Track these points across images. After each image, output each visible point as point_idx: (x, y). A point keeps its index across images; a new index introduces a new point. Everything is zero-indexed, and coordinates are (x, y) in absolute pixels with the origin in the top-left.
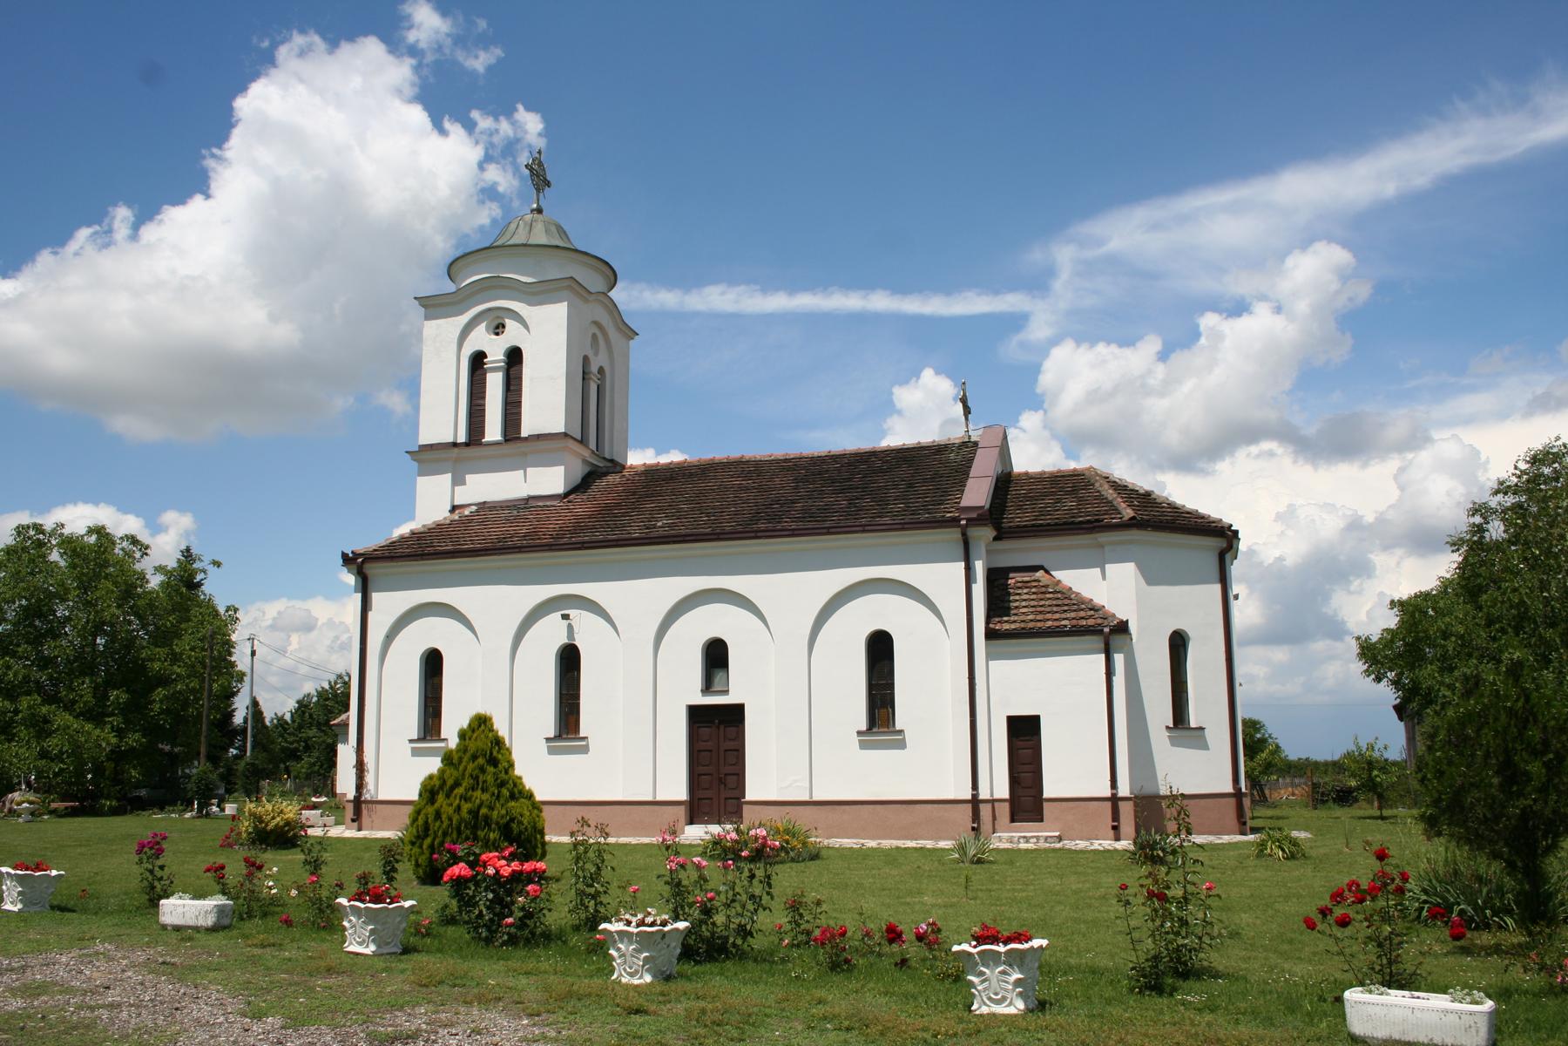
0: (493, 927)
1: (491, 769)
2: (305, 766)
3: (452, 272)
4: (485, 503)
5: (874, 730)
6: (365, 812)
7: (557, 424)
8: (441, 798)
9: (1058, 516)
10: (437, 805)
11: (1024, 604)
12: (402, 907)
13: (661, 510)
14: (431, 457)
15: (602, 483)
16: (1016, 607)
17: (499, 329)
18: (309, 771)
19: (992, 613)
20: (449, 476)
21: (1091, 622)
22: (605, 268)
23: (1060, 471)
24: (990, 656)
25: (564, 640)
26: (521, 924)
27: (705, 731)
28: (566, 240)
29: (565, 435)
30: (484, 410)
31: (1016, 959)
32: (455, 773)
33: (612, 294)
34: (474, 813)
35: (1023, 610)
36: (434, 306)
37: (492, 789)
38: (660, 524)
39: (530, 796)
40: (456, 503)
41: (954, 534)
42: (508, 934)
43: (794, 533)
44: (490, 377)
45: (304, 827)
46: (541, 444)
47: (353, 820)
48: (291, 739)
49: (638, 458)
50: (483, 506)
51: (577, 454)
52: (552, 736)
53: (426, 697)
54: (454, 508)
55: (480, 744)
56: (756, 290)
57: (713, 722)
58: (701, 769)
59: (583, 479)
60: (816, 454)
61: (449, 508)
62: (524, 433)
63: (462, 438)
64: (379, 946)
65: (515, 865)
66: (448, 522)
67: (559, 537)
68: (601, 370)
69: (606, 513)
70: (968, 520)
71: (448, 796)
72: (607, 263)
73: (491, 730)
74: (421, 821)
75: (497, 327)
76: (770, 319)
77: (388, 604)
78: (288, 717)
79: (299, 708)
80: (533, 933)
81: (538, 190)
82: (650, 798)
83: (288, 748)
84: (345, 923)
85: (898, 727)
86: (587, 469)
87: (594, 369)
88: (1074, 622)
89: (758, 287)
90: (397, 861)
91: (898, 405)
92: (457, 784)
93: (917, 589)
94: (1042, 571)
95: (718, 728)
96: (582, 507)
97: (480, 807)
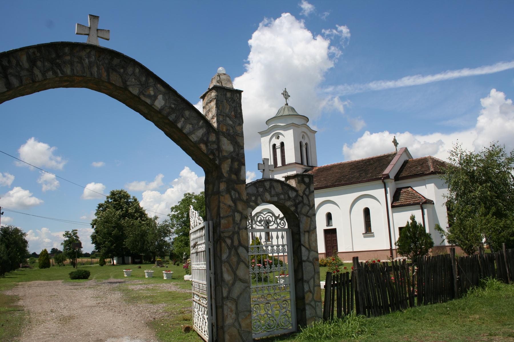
3: (267, 123)
5: (368, 233)
7: (293, 161)
9: (414, 172)
11: (403, 197)
16: (401, 199)
21: (418, 201)
22: (304, 117)
23: (421, 158)
24: (393, 212)
27: (328, 235)
28: (294, 111)
29: (296, 163)
33: (308, 124)
35: (403, 199)
41: (380, 182)
43: (343, 185)
51: (299, 167)
56: (419, 76)
62: (286, 164)
70: (384, 178)
72: (304, 116)
75: (278, 137)
76: (427, 85)
81: (286, 99)
82: (352, 251)
85: (372, 232)
87: (304, 144)
88: (414, 202)
89: (421, 75)
91: (483, 106)
94: (410, 188)
95: (331, 234)
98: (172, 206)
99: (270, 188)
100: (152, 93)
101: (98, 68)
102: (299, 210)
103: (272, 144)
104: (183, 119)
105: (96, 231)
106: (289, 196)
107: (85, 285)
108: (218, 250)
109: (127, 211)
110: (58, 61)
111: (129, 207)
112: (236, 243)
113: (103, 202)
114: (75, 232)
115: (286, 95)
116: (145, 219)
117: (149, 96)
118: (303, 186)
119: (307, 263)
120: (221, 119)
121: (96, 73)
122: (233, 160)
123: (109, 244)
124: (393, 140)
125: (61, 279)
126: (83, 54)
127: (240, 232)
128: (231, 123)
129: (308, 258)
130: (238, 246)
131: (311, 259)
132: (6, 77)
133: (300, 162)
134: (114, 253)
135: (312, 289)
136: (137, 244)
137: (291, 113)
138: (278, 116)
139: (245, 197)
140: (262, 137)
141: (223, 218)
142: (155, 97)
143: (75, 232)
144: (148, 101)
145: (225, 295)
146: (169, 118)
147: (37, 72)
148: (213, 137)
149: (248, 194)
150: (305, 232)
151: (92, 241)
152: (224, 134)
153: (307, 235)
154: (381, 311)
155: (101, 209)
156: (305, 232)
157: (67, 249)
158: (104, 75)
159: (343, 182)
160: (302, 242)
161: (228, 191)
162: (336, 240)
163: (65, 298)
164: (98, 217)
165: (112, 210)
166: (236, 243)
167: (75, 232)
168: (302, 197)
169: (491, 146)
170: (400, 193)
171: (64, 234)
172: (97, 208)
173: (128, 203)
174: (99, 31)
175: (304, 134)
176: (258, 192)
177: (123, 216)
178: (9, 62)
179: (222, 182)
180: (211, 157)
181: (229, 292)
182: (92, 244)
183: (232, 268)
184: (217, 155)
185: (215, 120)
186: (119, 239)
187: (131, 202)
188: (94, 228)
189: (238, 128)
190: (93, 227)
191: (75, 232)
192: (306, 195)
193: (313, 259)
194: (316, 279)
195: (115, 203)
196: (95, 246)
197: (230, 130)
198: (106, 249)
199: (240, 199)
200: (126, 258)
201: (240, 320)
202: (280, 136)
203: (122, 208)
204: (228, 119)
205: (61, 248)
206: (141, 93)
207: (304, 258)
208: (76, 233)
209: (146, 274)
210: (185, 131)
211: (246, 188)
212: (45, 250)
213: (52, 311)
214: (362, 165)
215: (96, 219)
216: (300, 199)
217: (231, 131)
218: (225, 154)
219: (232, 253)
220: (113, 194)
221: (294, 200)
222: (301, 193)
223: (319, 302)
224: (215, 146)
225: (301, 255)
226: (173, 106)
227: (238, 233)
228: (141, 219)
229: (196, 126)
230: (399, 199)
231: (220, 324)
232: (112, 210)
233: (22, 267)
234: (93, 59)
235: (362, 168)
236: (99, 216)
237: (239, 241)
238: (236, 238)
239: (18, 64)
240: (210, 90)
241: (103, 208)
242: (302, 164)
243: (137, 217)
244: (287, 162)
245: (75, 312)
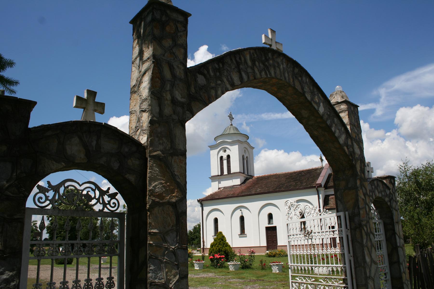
0: (217, 265)
2: (196, 242)
3: (215, 139)
4: (225, 187)
6: (205, 250)
7: (238, 170)
8: (214, 247)
10: (213, 248)
11: (332, 202)
12: (202, 262)
13: (259, 187)
14: (214, 178)
15: (248, 181)
16: (330, 203)
17: (225, 151)
18: (197, 243)
19: (325, 205)
20: (218, 182)
25: (241, 215)
26: (221, 265)
27: (269, 232)
29: (240, 172)
30: (223, 168)
31: (277, 265)
32: (216, 242)
33: (248, 141)
34: (219, 249)
36: (212, 147)
37: (222, 245)
38: (258, 190)
39: (229, 246)
40: (219, 187)
41: (315, 189)
42: (219, 266)
43: (283, 191)
44: (224, 161)
45: (192, 254)
47: (203, 252)
48: (193, 236)
50: (224, 188)
51: (242, 176)
52: (240, 234)
53: (215, 227)
54: (219, 188)
55: (220, 237)
57: (271, 230)
58: (269, 240)
59: (244, 181)
60: (291, 172)
61: (218, 188)
62: (232, 173)
63: (219, 174)
64: (199, 268)
65: (220, 256)
66: (218, 192)
67: (238, 194)
68: (247, 157)
69: (248, 188)
70: (318, 186)
71: (215, 246)
73: (222, 234)
74: (210, 251)
75: (225, 151)
77: (207, 209)
78: (192, 231)
79: (194, 228)
80: (222, 266)
81: (231, 120)
82: (259, 246)
83: (192, 238)
84: (195, 265)
86: (245, 178)
87: (245, 157)
90: (204, 257)
92: (216, 244)
93: (275, 205)
95: (272, 231)
96: (244, 187)
97: (220, 248)
98: (101, 205)
101: (288, 73)
103: (219, 156)
115: (231, 117)
121: (287, 78)
133: (243, 172)
143: (35, 222)
151: (46, 231)
159: (282, 189)
169: (427, 164)
170: (329, 199)
174: (277, 43)
182: (47, 234)
188: (49, 220)
191: (35, 222)
196: (49, 236)
202: (227, 150)
208: (36, 224)
230: (329, 204)
235: (296, 178)
241: (58, 203)
244: (232, 171)
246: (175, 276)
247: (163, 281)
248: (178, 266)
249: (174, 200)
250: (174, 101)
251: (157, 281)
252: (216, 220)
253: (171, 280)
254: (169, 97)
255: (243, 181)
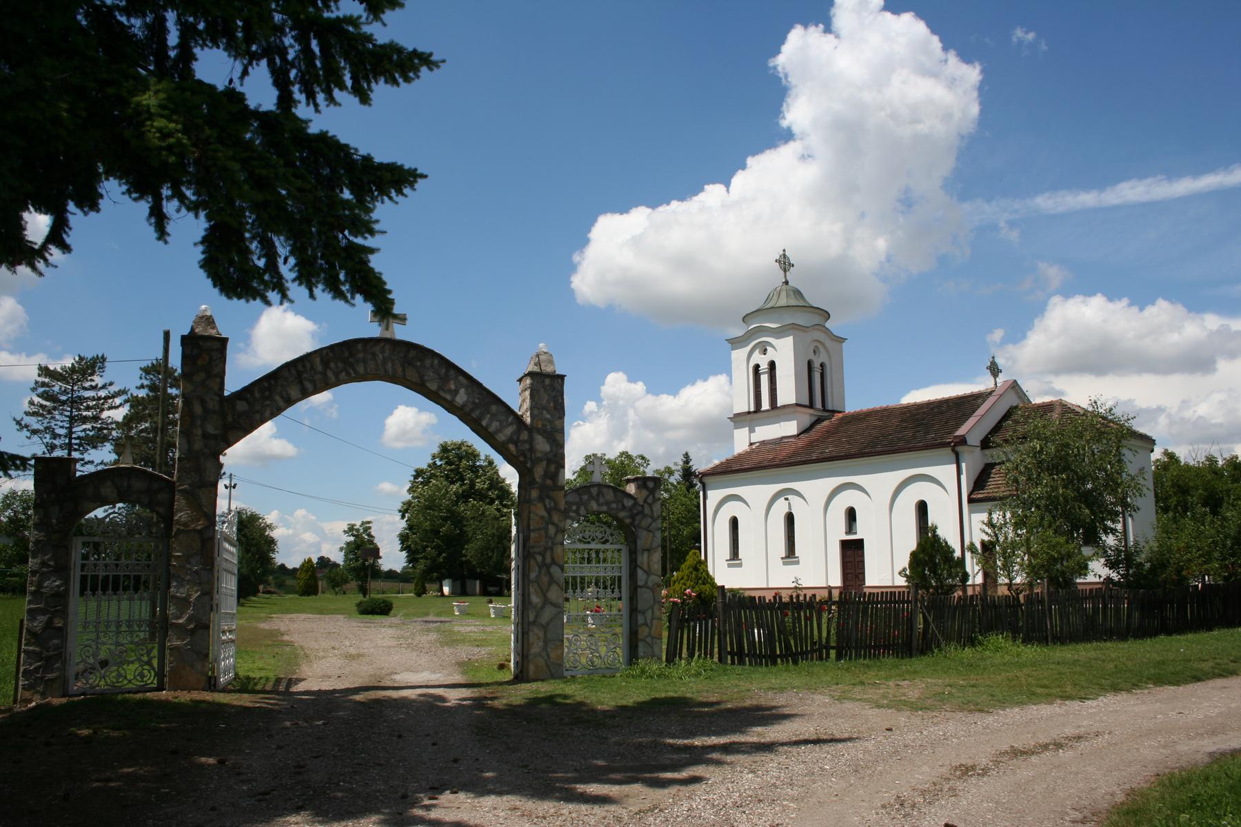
1: (694, 573)
7: (792, 400)
15: (818, 426)
17: (765, 352)
22: (821, 312)
24: (971, 512)
27: (849, 553)
29: (797, 405)
44: (762, 376)
46: (786, 410)
49: (853, 404)
51: (807, 413)
54: (751, 444)
56: (1163, 180)
58: (849, 571)
69: (811, 445)
81: (785, 271)
82: (765, 586)
87: (817, 365)
99: (598, 495)
100: (453, 387)
102: (636, 523)
103: (752, 364)
104: (489, 416)
105: (409, 525)
106: (623, 505)
107: (382, 623)
108: (527, 567)
109: (472, 484)
110: (351, 360)
111: (477, 477)
112: (548, 560)
113: (424, 466)
114: (366, 526)
115: (785, 263)
116: (509, 503)
117: (450, 391)
118: (645, 493)
119: (644, 590)
120: (536, 412)
122: (549, 461)
123: (434, 553)
124: (989, 364)
125: (343, 614)
126: (377, 349)
127: (554, 548)
128: (549, 416)
129: (646, 582)
130: (551, 564)
131: (650, 584)
132: (301, 383)
133: (807, 403)
134: (443, 571)
135: (649, 622)
136: (490, 554)
137: (793, 302)
138: (768, 306)
139: (562, 506)
140: (733, 349)
141: (533, 531)
142: (456, 392)
144: (448, 397)
145: (531, 618)
146: (473, 415)
147: (330, 374)
148: (524, 436)
149: (566, 503)
150: (644, 550)
152: (538, 431)
153: (646, 554)
154: (761, 661)
155: (420, 479)
156: (644, 550)
157: (351, 560)
158: (400, 370)
159: (879, 448)
160: (639, 563)
161: (541, 499)
162: (863, 562)
163: (351, 636)
164: (413, 497)
165: (442, 484)
166: (548, 560)
167: (366, 526)
168: (642, 506)
170: (990, 473)
171: (346, 529)
172: (412, 479)
173: (474, 469)
175: (817, 344)
176: (581, 499)
177: (464, 497)
178: (304, 366)
179: (533, 488)
180: (521, 459)
181: (537, 616)
183: (542, 590)
184: (529, 457)
185: (528, 414)
186: (455, 542)
187: (481, 466)
188: (405, 519)
189: (557, 423)
190: (403, 517)
192: (648, 504)
193: (653, 585)
194: (655, 610)
195: (448, 468)
197: (546, 426)
198: (428, 562)
199: (556, 508)
200: (469, 582)
201: (549, 649)
203: (462, 479)
204: (545, 412)
205: (338, 557)
206: (440, 388)
207: (640, 583)
208: (370, 528)
209: (492, 611)
210: (491, 429)
211: (565, 496)
212: (310, 560)
213: (333, 648)
214: (924, 413)
215: (410, 501)
216: (640, 508)
217: (548, 427)
218: (539, 455)
219: (543, 572)
220: (445, 449)
221: (631, 510)
222: (641, 501)
223: (658, 639)
224: (527, 446)
225: (637, 579)
226: (477, 401)
227: (552, 549)
228: (501, 503)
229: (505, 423)
231: (525, 654)
232: (442, 484)
233: (263, 593)
234: (387, 353)
236: (415, 495)
237: (553, 559)
238: (548, 554)
239: (312, 368)
240: (526, 375)
241: (423, 478)
242: (811, 405)
243: (491, 498)
245: (365, 651)
246: (196, 592)
247: (184, 595)
248: (200, 584)
249: (199, 528)
250: (205, 436)
251: (178, 595)
252: (734, 523)
253: (191, 595)
254: (199, 432)
255: (809, 425)
